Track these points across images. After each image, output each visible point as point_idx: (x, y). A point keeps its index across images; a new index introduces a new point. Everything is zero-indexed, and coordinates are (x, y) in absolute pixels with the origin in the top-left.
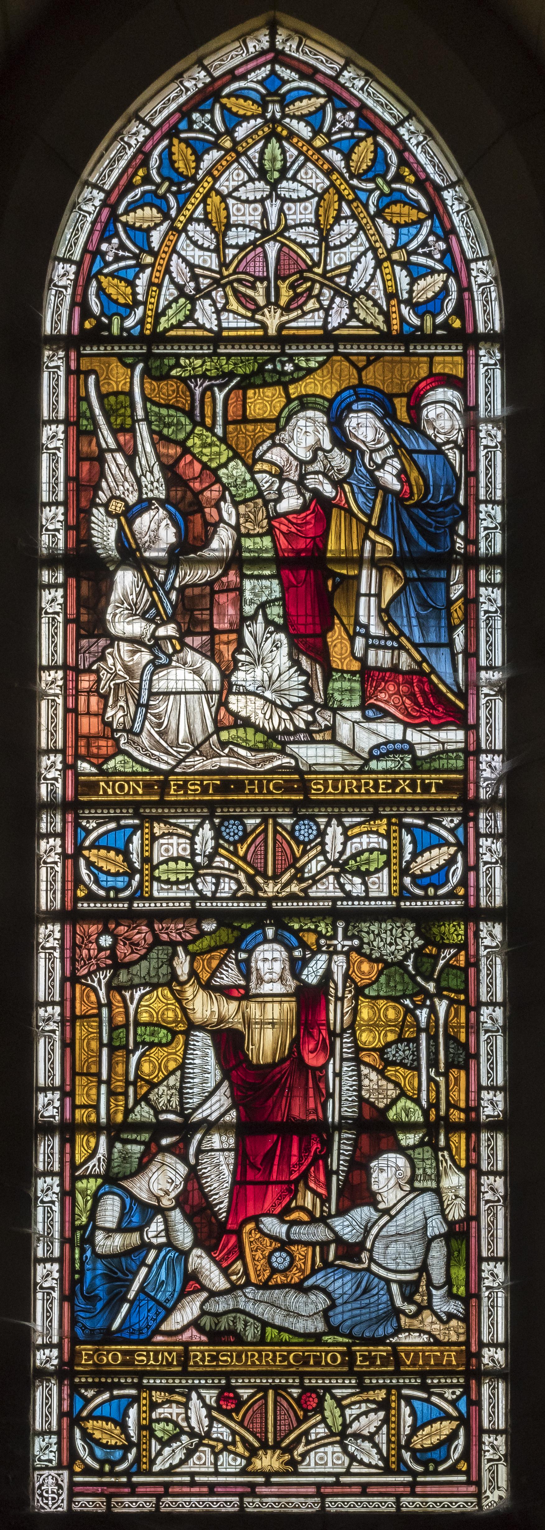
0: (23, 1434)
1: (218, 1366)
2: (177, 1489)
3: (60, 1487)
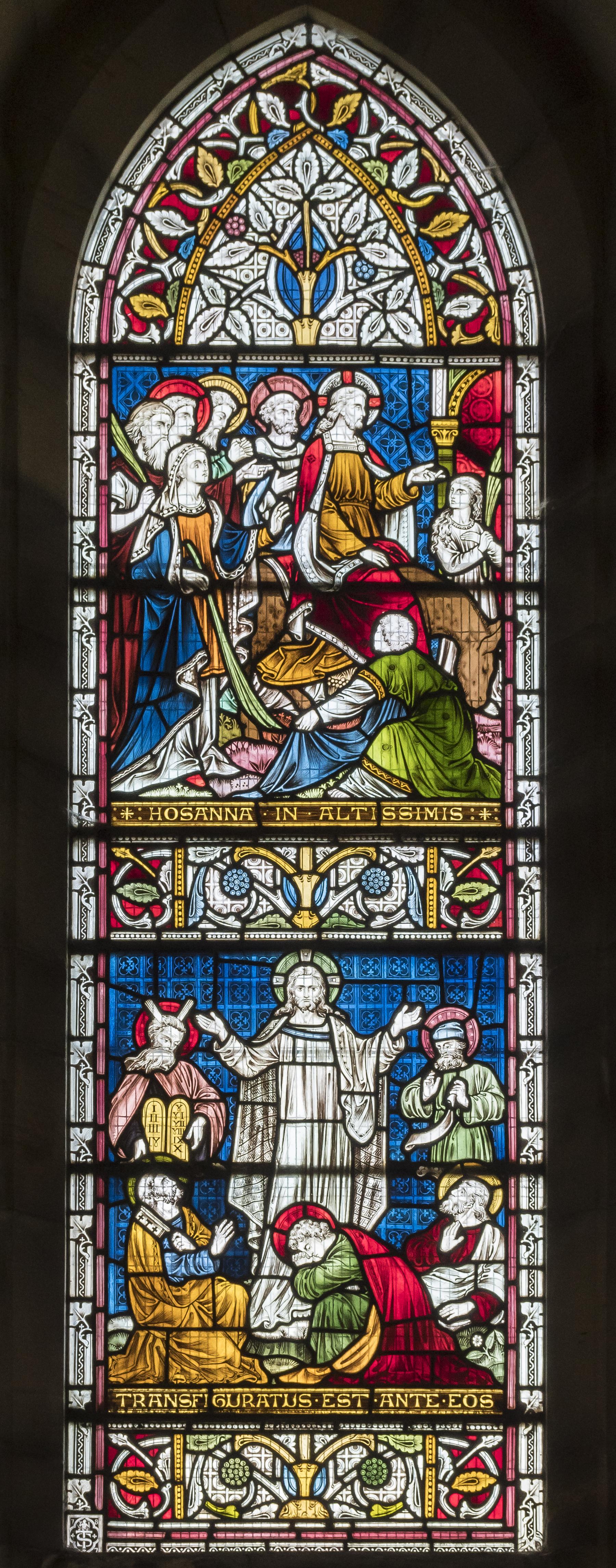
0: (58, 1475)
1: (336, 1408)
2: (481, 1535)
3: (95, 1532)
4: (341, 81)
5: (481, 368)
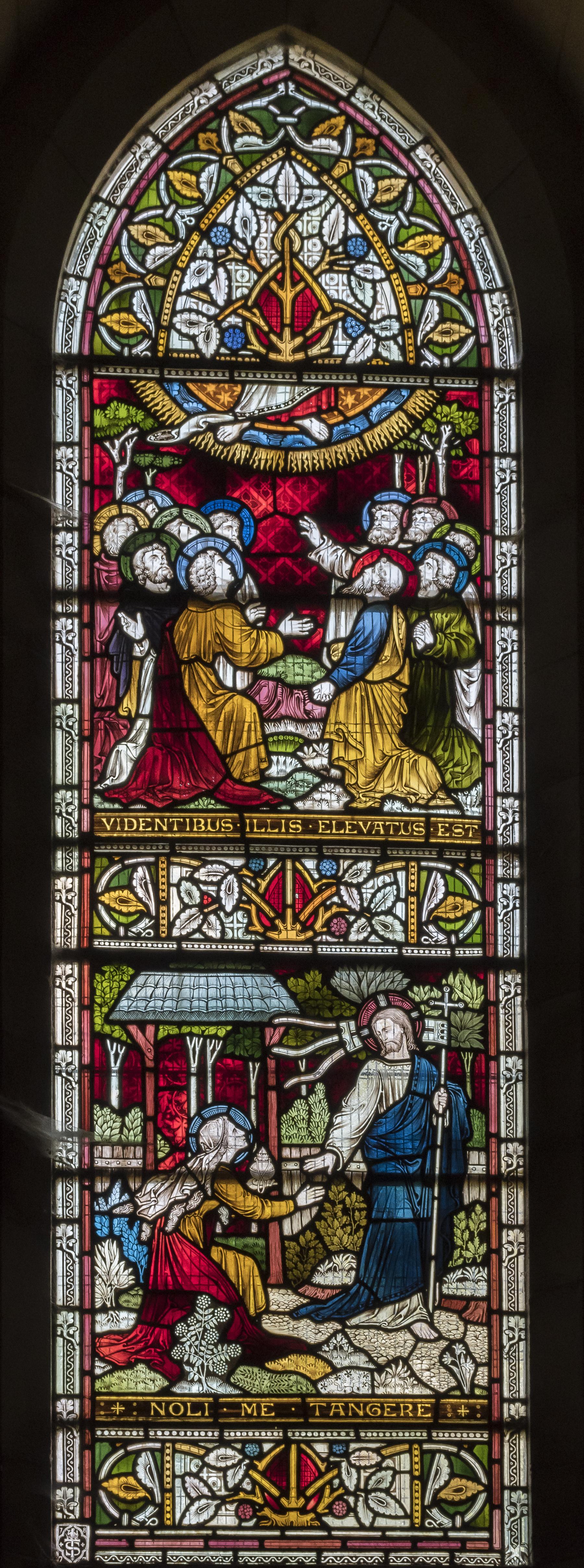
3: (83, 1540)
4: (324, 106)
5: (315, 385)
